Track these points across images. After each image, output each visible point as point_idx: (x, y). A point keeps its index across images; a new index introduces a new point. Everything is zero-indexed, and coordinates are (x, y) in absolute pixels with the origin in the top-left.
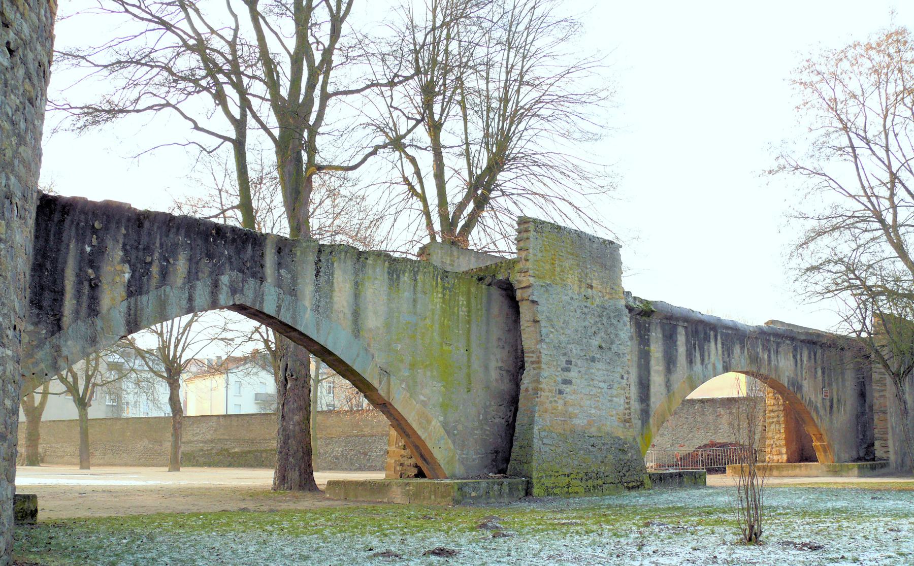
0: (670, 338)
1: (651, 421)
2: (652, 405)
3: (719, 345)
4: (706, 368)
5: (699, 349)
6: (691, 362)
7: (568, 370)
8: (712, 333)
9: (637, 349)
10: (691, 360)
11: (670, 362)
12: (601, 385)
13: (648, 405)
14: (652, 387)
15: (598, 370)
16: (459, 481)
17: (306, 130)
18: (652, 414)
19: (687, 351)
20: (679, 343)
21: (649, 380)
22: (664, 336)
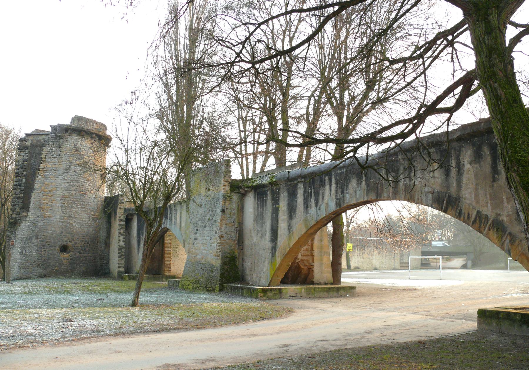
0: (292, 195)
1: (277, 253)
2: (278, 243)
3: (334, 186)
4: (320, 209)
5: (315, 195)
6: (307, 206)
7: (196, 233)
8: (327, 178)
9: (271, 208)
10: (307, 205)
11: (292, 210)
12: (207, 238)
13: (276, 244)
14: (279, 231)
15: (207, 231)
16: (262, 287)
17: (507, 46)
18: (278, 249)
19: (304, 200)
20: (299, 195)
21: (277, 227)
22: (288, 194)
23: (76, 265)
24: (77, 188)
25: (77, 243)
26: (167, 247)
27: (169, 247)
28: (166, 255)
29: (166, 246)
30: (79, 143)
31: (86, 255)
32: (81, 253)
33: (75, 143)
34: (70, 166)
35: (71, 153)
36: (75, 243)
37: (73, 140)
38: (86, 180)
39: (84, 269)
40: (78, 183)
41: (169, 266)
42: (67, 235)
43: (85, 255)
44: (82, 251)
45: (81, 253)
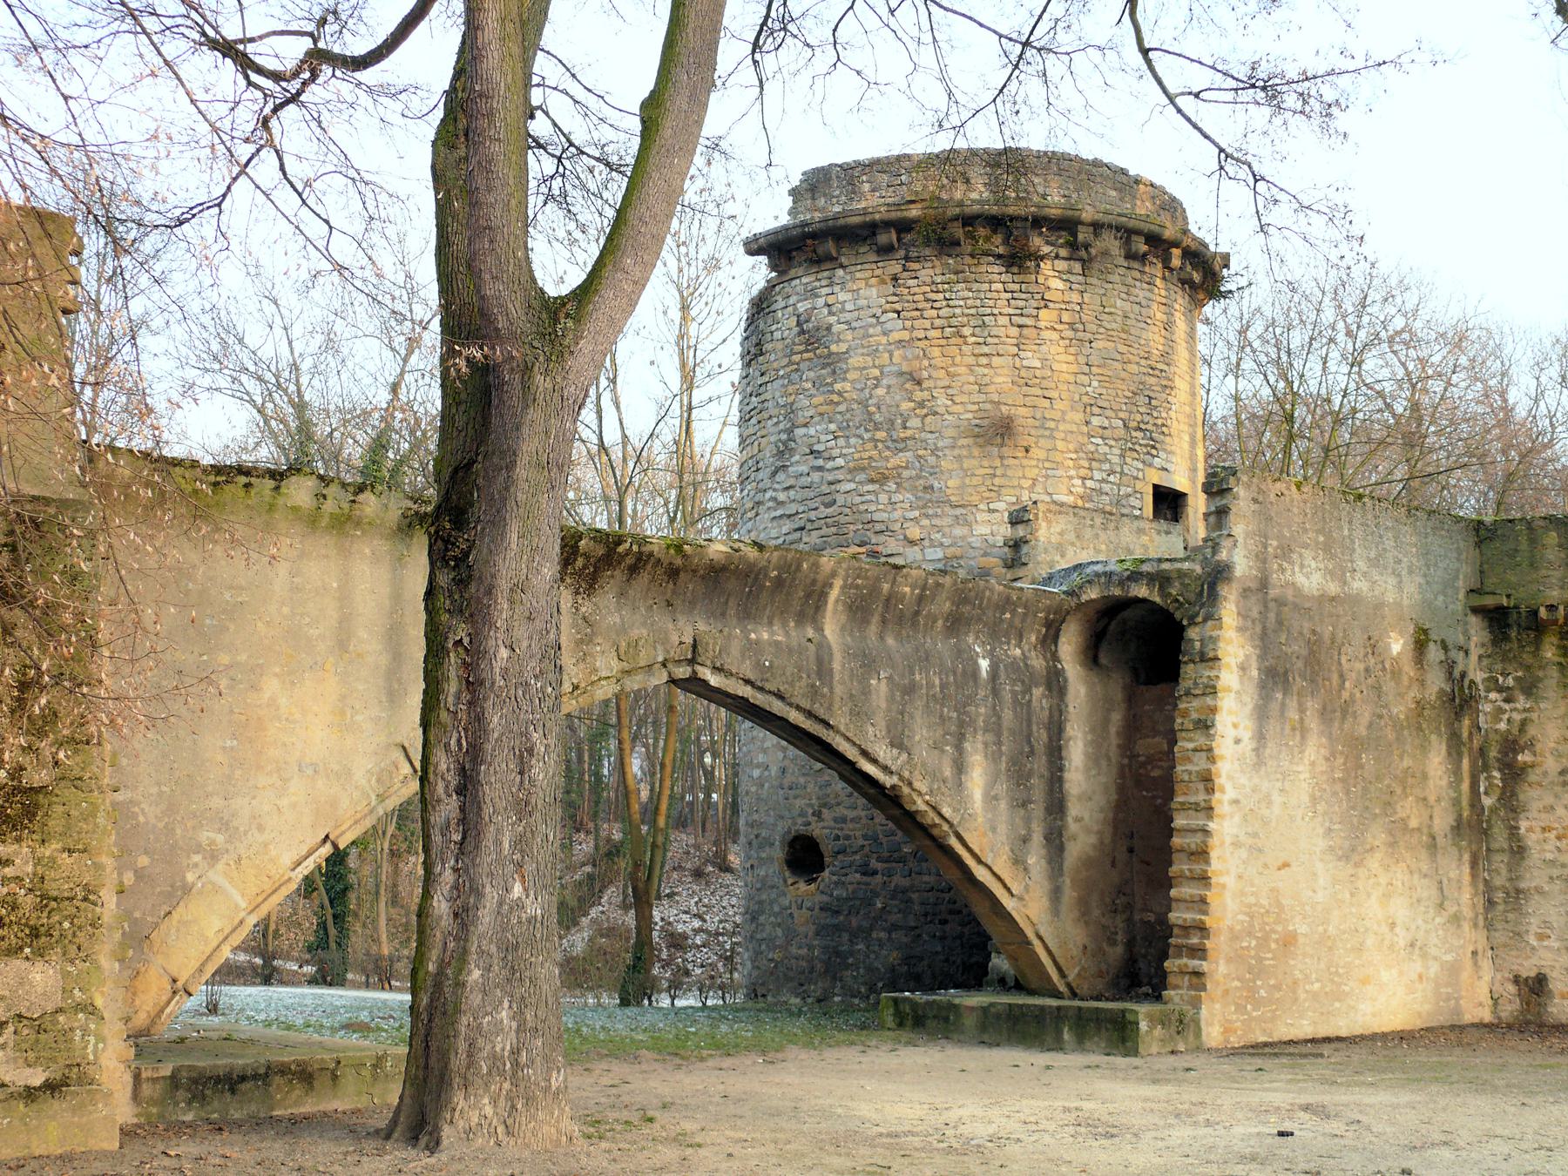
23: (846, 936)
24: (825, 531)
25: (844, 820)
26: (1185, 807)
27: (1196, 807)
28: (1180, 866)
29: (1179, 799)
30: (820, 302)
31: (906, 882)
32: (875, 873)
33: (802, 307)
34: (790, 431)
35: (791, 363)
36: (835, 820)
37: (792, 300)
38: (872, 481)
39: (894, 957)
40: (827, 505)
41: (1195, 940)
42: (802, 780)
43: (898, 880)
44: (879, 860)
45: (875, 873)
